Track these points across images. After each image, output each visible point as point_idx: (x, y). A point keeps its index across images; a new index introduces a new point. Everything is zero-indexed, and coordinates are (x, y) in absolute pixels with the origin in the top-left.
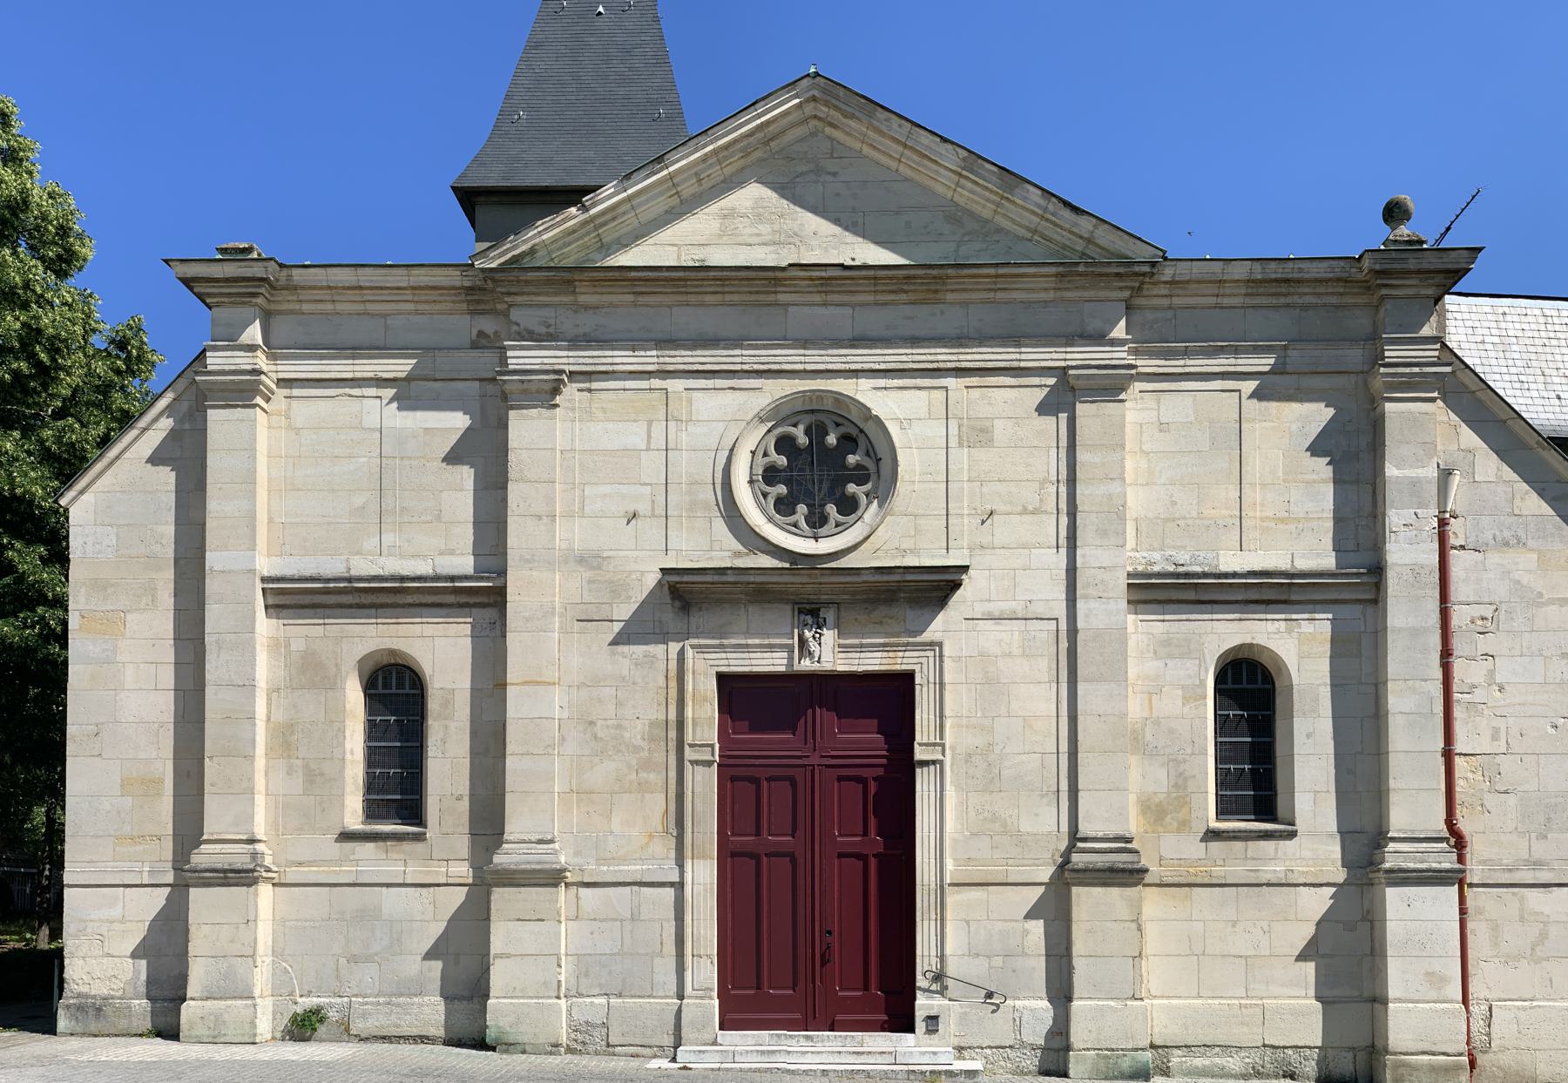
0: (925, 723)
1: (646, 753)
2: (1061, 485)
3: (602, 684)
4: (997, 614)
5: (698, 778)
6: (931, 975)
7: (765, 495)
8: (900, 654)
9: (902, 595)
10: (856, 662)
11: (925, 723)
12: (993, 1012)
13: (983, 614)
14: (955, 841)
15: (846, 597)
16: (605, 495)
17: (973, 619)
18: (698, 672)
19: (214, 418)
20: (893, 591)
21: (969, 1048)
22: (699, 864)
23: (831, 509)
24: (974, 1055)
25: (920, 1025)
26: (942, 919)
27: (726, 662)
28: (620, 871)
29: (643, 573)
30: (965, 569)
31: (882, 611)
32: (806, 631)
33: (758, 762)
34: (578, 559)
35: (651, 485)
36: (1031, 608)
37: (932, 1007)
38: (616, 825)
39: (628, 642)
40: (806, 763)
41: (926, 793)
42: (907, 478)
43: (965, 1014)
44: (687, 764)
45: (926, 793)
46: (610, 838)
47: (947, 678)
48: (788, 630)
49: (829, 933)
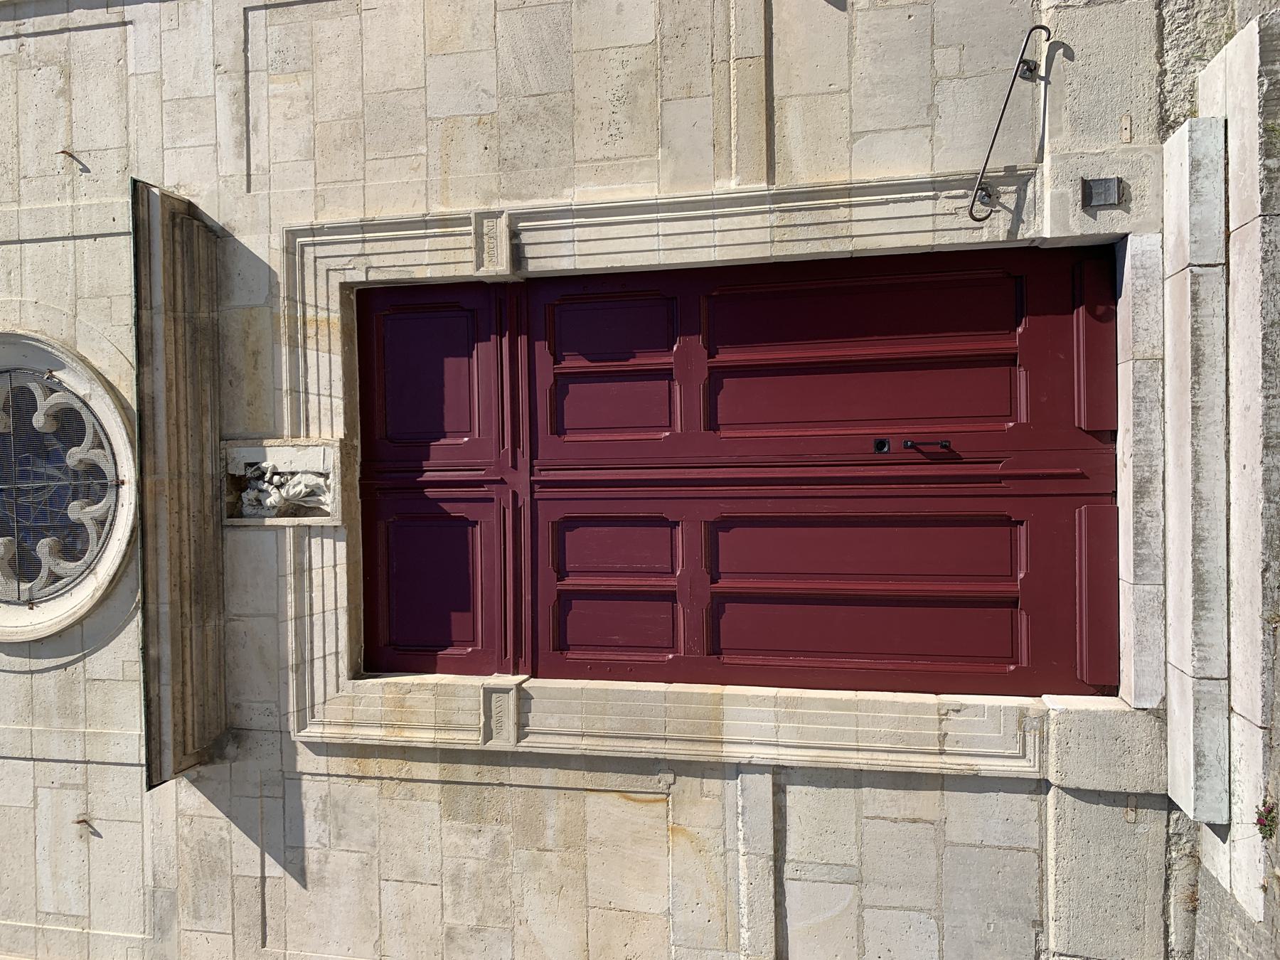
0: (439, 257)
1: (508, 828)
2: (22, 30)
3: (376, 909)
4: (238, 129)
5: (553, 723)
6: (980, 209)
7: (55, 578)
8: (310, 312)
9: (204, 315)
10: (326, 401)
11: (439, 257)
12: (1069, 55)
13: (239, 156)
14: (675, 179)
15: (208, 424)
16: (54, 874)
17: (249, 175)
18: (349, 716)
19: (695, 783)
20: (195, 330)
21: (1162, 103)
22: (733, 726)
23: (75, 456)
24: (1180, 91)
25: (1106, 224)
26: (849, 191)
27: (331, 661)
28: (750, 904)
29: (179, 813)
30: (138, 189)
31: (235, 354)
32: (269, 501)
33: (527, 597)
34: (158, 935)
35: (35, 789)
36: (226, 64)
37: (1059, 199)
38: (651, 901)
39: (300, 848)
40: (528, 499)
41: (579, 248)
42: (14, 317)
43: (1075, 121)
44: (524, 746)
45: (579, 248)
46: (679, 917)
47: (354, 216)
48: (270, 536)
49: (880, 445)
